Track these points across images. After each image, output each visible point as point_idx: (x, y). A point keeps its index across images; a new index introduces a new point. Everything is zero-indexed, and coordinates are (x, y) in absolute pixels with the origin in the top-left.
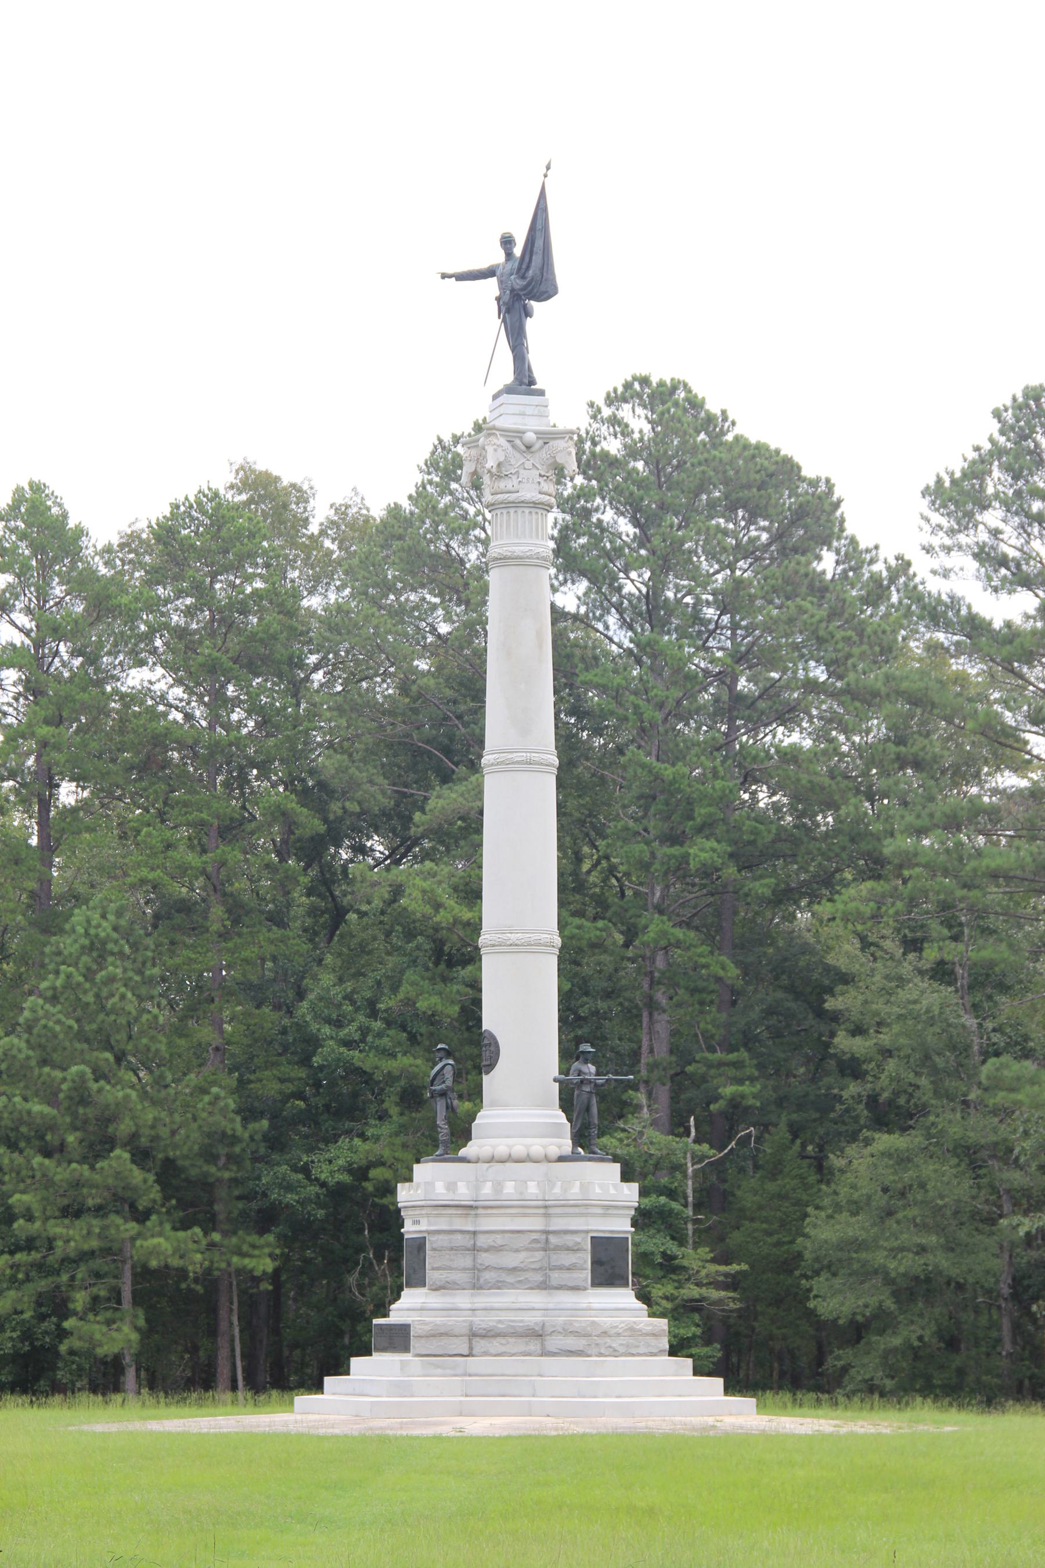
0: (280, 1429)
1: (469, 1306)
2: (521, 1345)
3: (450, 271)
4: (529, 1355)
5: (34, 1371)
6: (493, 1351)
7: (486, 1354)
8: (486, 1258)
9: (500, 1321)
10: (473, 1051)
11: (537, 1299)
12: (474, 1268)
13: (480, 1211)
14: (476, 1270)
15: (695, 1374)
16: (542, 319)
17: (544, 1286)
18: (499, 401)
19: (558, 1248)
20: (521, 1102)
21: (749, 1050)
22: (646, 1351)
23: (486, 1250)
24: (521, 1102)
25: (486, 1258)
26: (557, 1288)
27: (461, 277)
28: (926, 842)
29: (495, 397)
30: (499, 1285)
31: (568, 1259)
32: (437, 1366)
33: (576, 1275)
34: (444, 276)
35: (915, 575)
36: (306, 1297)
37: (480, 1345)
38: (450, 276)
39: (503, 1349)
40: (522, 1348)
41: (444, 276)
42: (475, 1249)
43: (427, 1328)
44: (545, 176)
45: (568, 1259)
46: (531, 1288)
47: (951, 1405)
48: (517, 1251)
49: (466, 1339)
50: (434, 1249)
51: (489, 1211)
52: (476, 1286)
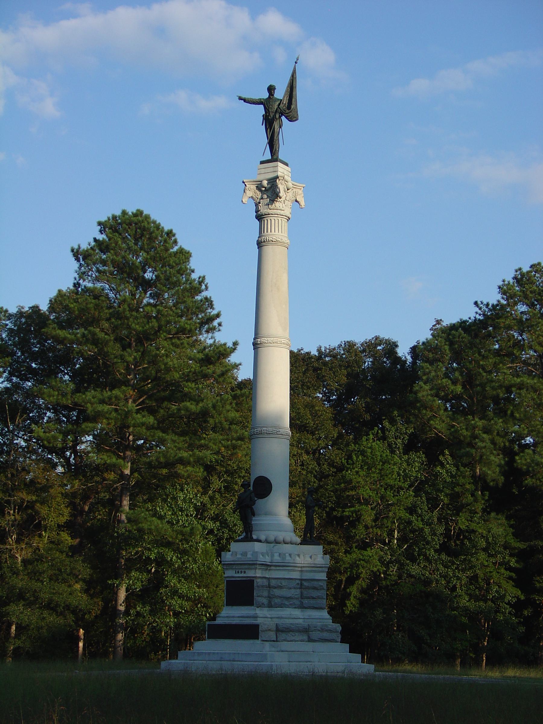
2: (298, 636)
3: (243, 96)
6: (289, 639)
7: (285, 640)
8: (277, 592)
11: (297, 613)
12: (269, 597)
13: (272, 568)
16: (287, 129)
17: (302, 607)
19: (308, 588)
23: (275, 588)
25: (277, 592)
26: (306, 608)
27: (245, 100)
30: (281, 606)
31: (315, 594)
33: (319, 601)
34: (240, 98)
35: (509, 282)
37: (283, 636)
38: (242, 99)
39: (293, 638)
40: (301, 638)
42: (269, 586)
44: (296, 63)
45: (315, 594)
46: (295, 608)
47: (343, 672)
50: (258, 587)
51: (278, 568)
52: (270, 606)
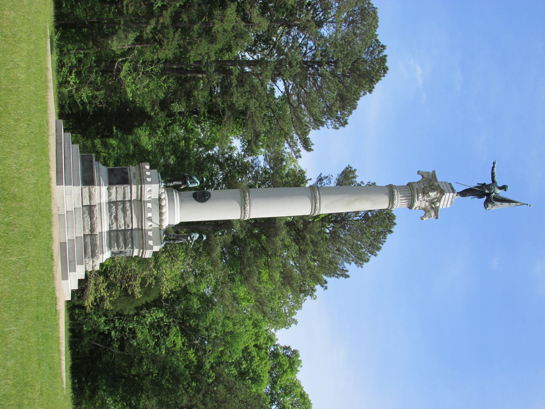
0: (69, 374)
1: (102, 202)
4: (84, 230)
5: (69, 27)
9: (97, 218)
10: (201, 196)
14: (116, 203)
15: (79, 280)
18: (448, 186)
20: (180, 212)
21: (214, 61)
22: (85, 225)
24: (180, 212)
25: (120, 207)
27: (493, 167)
28: (326, 31)
29: (450, 184)
32: (78, 198)
34: (494, 163)
36: (101, 129)
41: (494, 163)
43: (93, 192)
48: (124, 219)
49: (89, 204)
